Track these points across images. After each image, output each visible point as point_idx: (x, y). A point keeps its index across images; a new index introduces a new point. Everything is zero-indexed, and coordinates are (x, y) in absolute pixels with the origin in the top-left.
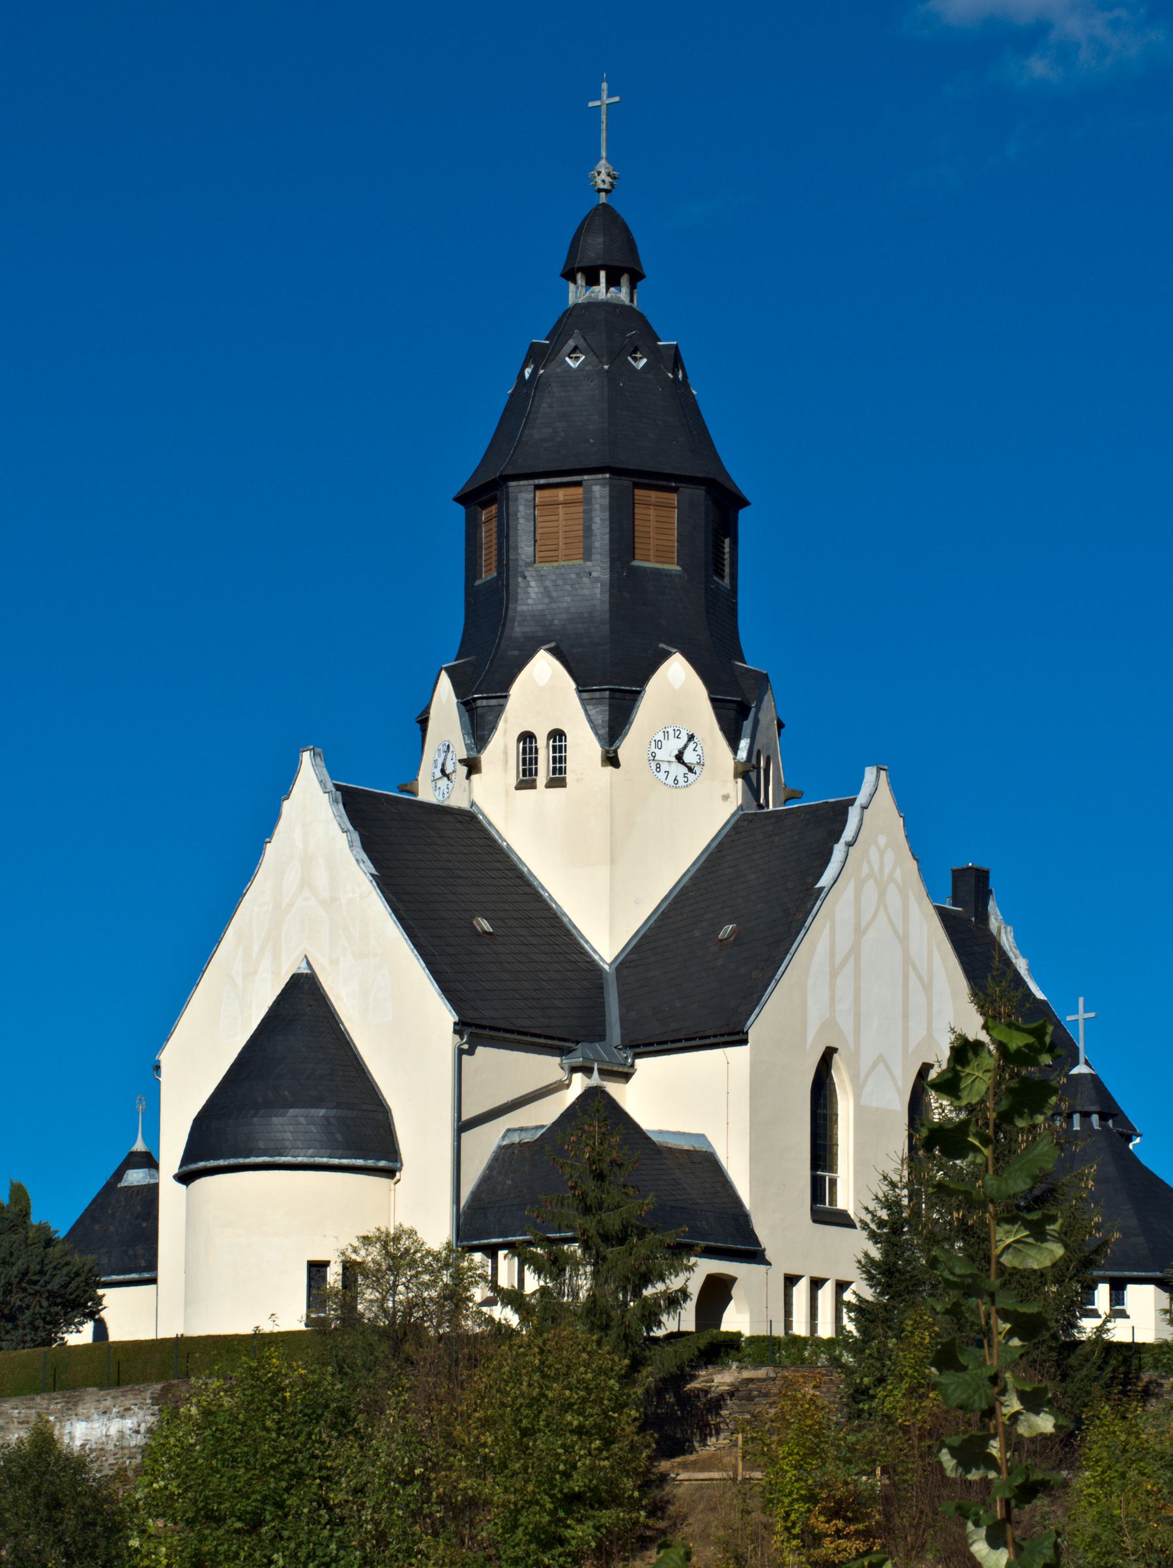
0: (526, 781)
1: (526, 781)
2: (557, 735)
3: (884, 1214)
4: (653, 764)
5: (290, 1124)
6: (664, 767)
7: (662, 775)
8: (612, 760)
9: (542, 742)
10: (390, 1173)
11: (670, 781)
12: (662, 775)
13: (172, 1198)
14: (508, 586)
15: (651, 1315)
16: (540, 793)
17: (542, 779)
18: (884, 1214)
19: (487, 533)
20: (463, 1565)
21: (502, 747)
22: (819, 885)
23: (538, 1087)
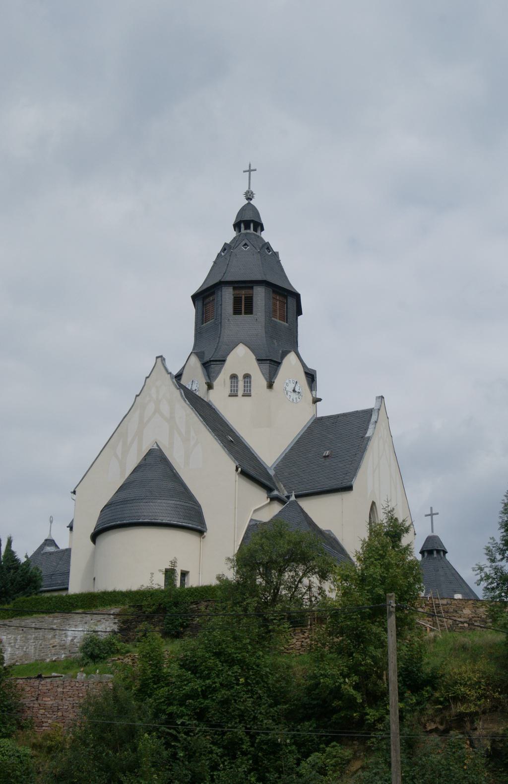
0: (233, 395)
1: (233, 395)
2: (247, 376)
3: (503, 542)
4: (285, 392)
5: (266, 366)
6: (289, 393)
7: (288, 397)
8: (270, 386)
9: (240, 378)
10: (200, 532)
11: (291, 400)
12: (288, 397)
14: (221, 323)
16: (240, 399)
17: (240, 392)
18: (503, 542)
20: (213, 780)
22: (367, 435)
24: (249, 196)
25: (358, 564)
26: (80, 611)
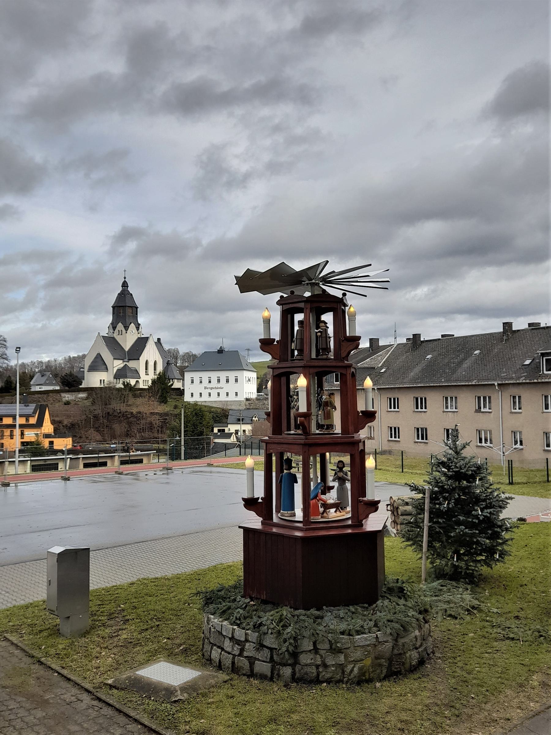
13: (86, 372)
21: (116, 330)
23: (119, 364)
24: (125, 278)
26: (212, 410)
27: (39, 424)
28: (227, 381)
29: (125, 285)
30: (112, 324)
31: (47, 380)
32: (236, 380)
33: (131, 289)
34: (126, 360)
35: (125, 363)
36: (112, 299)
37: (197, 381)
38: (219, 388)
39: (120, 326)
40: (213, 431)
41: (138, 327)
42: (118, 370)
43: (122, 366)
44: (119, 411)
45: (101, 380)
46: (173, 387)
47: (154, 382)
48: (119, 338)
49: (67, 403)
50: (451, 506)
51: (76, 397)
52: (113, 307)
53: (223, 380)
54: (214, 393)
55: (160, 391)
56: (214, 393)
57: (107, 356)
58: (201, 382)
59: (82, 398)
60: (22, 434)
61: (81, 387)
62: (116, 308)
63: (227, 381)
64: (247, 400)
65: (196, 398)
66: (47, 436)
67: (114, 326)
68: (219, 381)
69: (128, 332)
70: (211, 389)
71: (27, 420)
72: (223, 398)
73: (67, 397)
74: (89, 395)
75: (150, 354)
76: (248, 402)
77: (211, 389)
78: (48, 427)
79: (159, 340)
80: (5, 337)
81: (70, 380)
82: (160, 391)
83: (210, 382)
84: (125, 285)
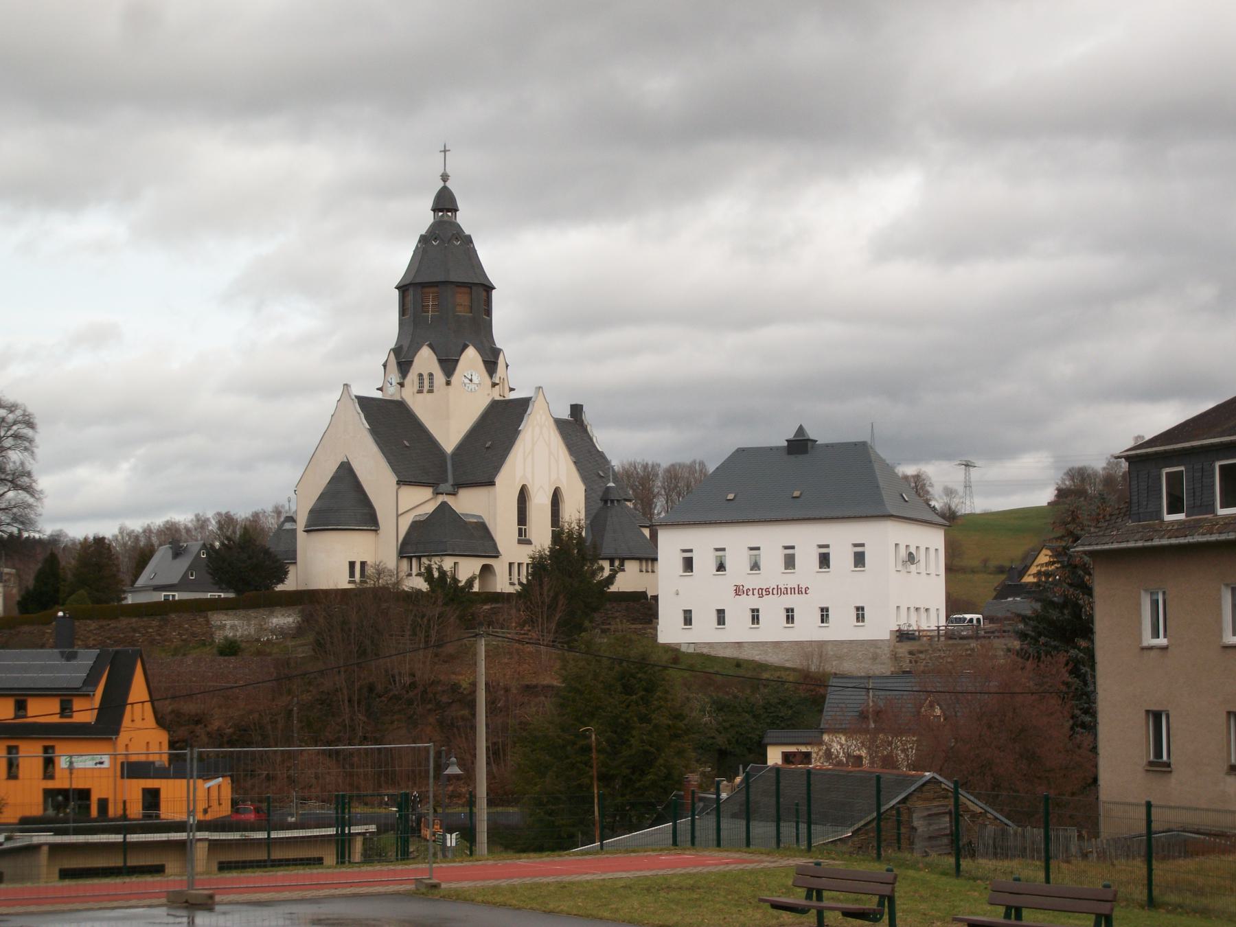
0: (420, 392)
2: (431, 375)
13: (301, 536)
15: (594, 574)
16: (426, 396)
19: (1173, 898)
21: (412, 376)
23: (419, 501)
24: (445, 178)
25: (909, 470)
26: (765, 675)
27: (107, 725)
28: (824, 560)
29: (445, 203)
30: (397, 351)
31: (191, 568)
32: (859, 559)
33: (465, 219)
34: (446, 487)
35: (441, 499)
36: (397, 259)
37: (704, 562)
38: (793, 591)
39: (425, 360)
40: (764, 759)
41: (491, 360)
42: (415, 525)
43: (430, 508)
44: (407, 680)
45: (352, 564)
46: (613, 589)
47: (539, 567)
48: (421, 406)
49: (231, 649)
50: (458, 308)
51: (261, 629)
52: (403, 288)
53: (807, 558)
54: (772, 609)
55: (562, 600)
56: (772, 609)
57: (375, 474)
58: (721, 567)
59: (282, 632)
60: (49, 763)
61: (280, 588)
62: (411, 292)
63: (824, 560)
64: (903, 636)
65: (703, 634)
66: (133, 770)
67: (403, 359)
68: (790, 562)
69: (455, 379)
70: (763, 592)
71: (66, 709)
72: (807, 629)
73: (232, 626)
74: (307, 619)
75: (539, 463)
76: (903, 649)
77: (763, 592)
78: (143, 735)
79: (576, 410)
80: (30, 410)
81: (245, 560)
82: (562, 600)
83: (755, 566)
84: (445, 203)
